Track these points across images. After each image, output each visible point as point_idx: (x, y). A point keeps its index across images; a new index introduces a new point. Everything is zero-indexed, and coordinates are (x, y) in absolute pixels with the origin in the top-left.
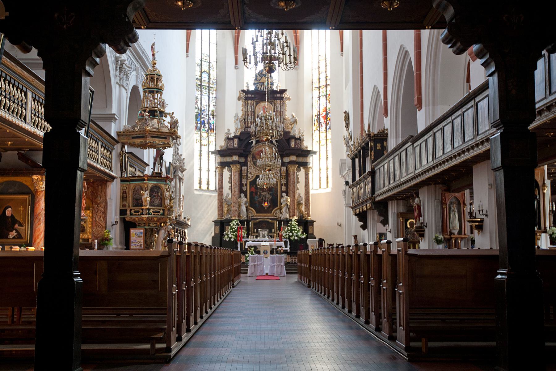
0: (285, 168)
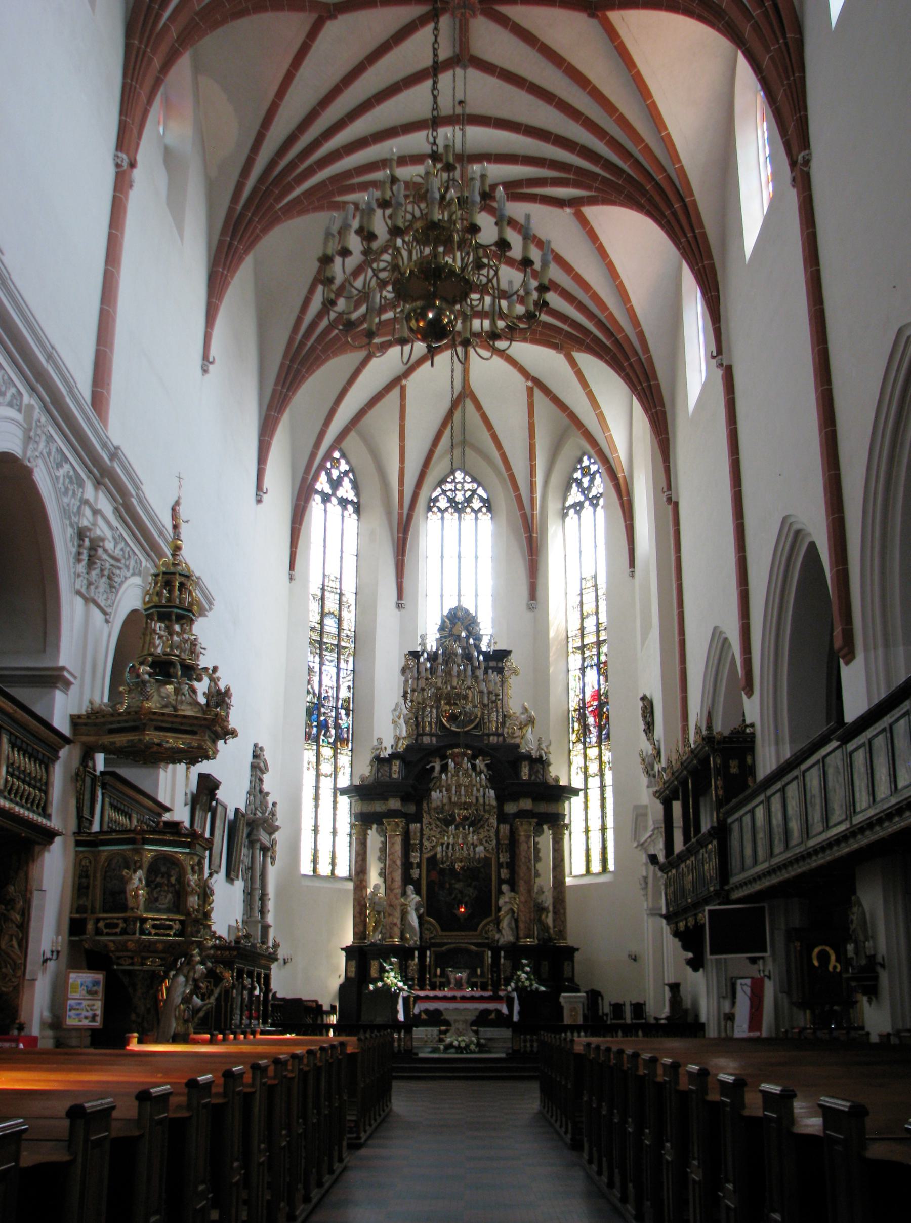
0: (507, 827)
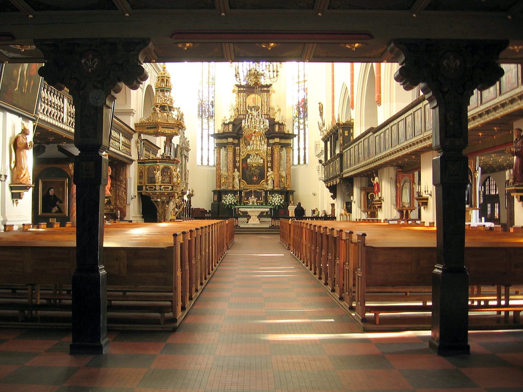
0: (271, 148)
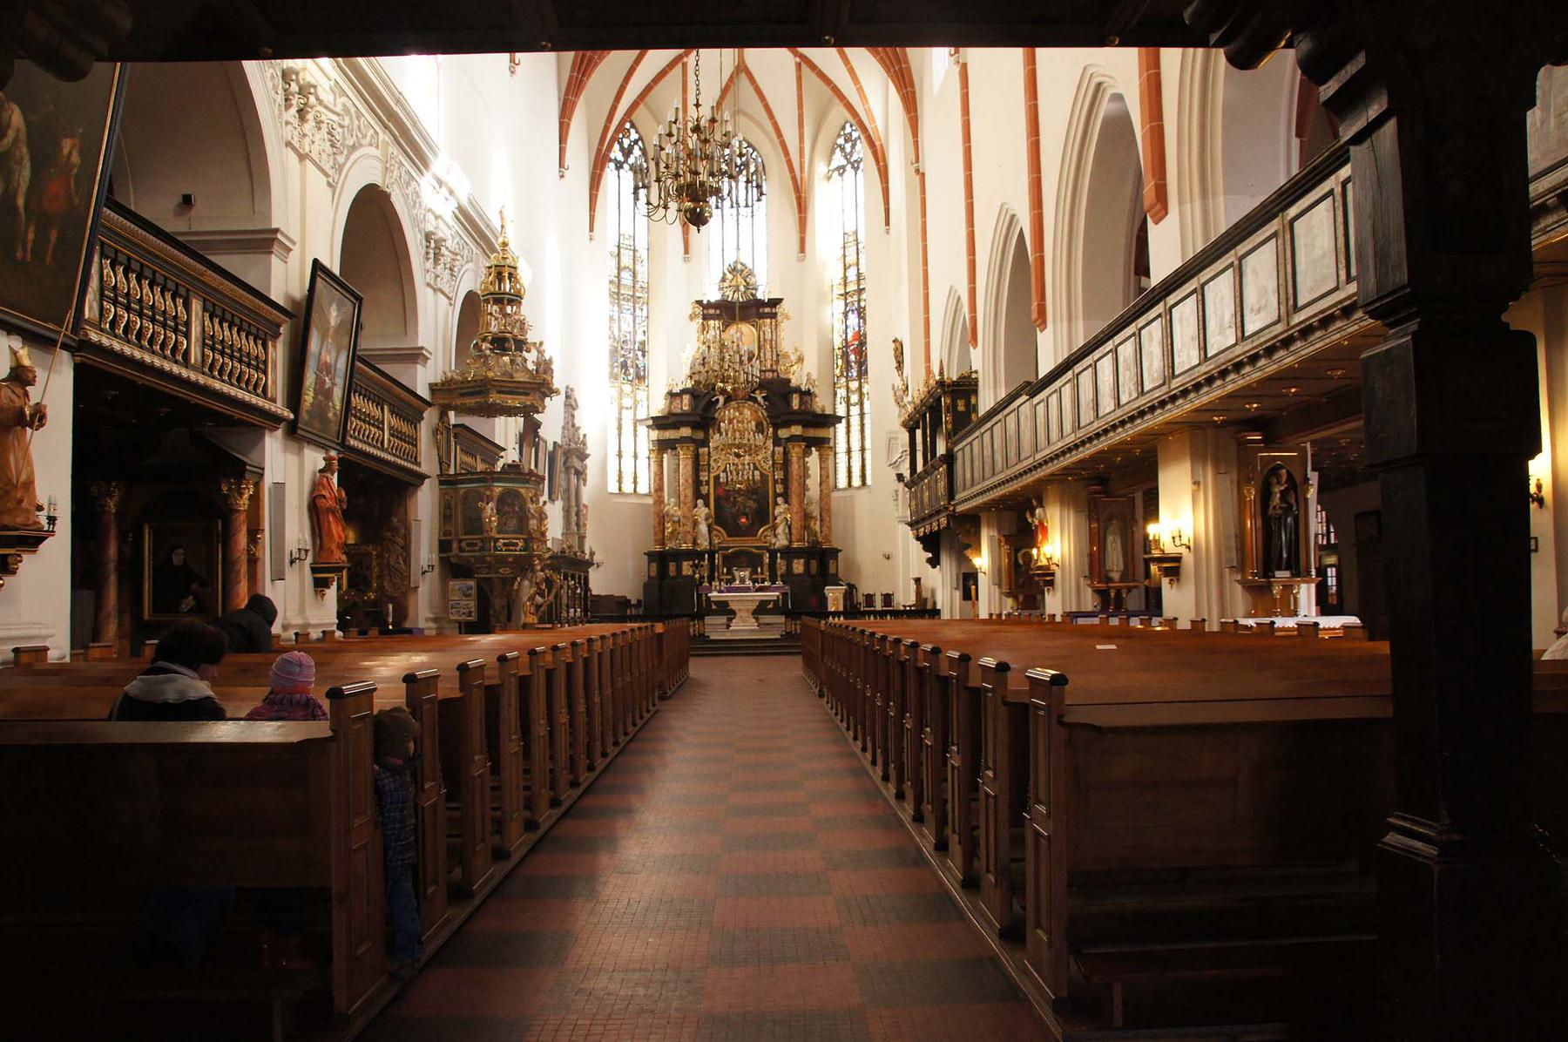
0: (781, 449)
